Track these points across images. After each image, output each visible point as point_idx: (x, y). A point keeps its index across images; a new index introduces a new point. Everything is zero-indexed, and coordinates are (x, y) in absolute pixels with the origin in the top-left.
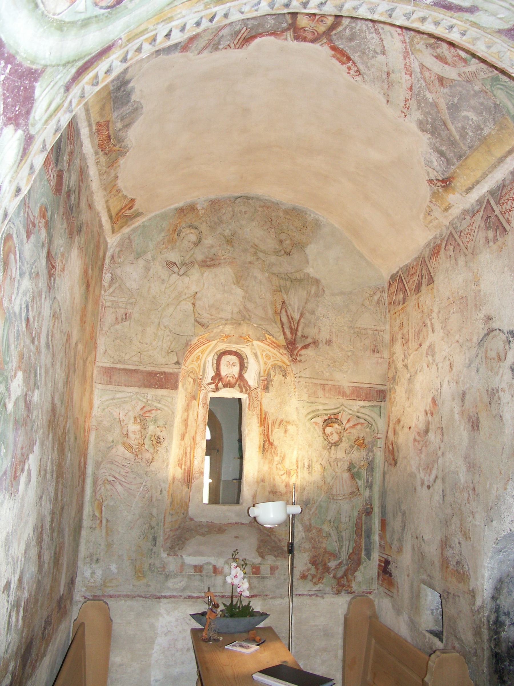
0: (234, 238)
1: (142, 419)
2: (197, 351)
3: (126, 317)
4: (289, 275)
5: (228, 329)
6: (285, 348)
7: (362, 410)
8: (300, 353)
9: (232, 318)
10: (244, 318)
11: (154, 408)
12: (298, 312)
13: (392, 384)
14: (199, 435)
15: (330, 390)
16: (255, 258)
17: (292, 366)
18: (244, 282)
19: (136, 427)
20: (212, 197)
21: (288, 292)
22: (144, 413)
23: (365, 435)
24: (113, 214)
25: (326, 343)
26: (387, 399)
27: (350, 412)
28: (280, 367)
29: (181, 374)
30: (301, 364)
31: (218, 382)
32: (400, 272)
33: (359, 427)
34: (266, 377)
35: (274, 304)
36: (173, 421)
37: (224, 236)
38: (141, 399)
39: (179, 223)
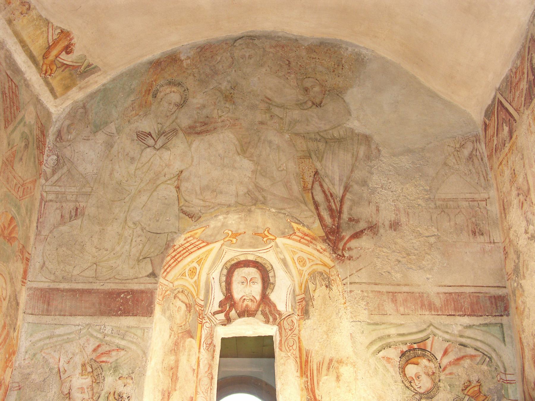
0: (235, 92)
1: (95, 368)
2: (189, 259)
3: (77, 213)
4: (321, 134)
5: (233, 220)
6: (324, 241)
7: (469, 333)
8: (348, 246)
9: (237, 202)
10: (255, 202)
11: (115, 348)
12: (340, 185)
13: (515, 281)
14: (202, 395)
15: (405, 300)
16: (268, 115)
17: (337, 267)
18: (253, 151)
19: (84, 381)
20: (200, 39)
21: (322, 157)
22: (98, 357)
23: (482, 377)
24: (37, 53)
25: (391, 227)
26: (512, 311)
27: (447, 337)
28: (321, 274)
29: (158, 292)
30: (352, 263)
31: (230, 310)
32: (499, 96)
33: (467, 363)
34: (303, 296)
35: (301, 176)
36: (144, 368)
37: (221, 91)
38: (95, 334)
39: (155, 81)
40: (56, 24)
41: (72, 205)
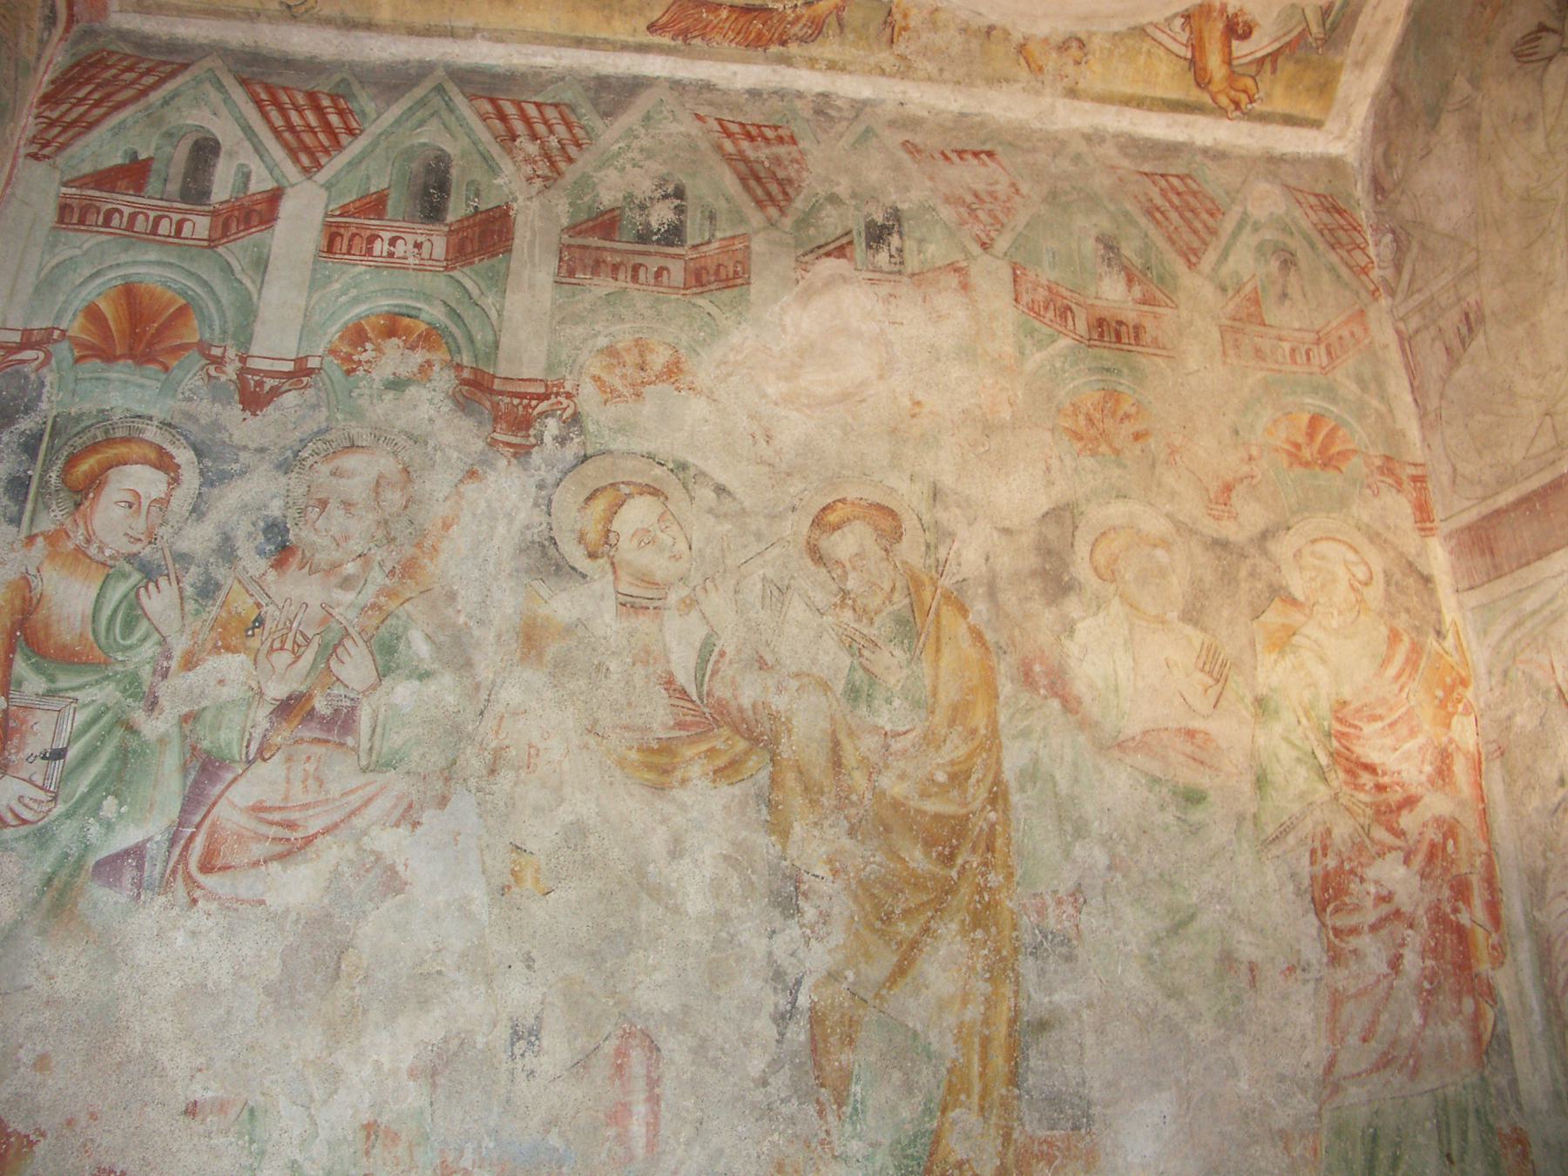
3: (1471, 323)
40: (1158, 18)
41: (1454, 315)
